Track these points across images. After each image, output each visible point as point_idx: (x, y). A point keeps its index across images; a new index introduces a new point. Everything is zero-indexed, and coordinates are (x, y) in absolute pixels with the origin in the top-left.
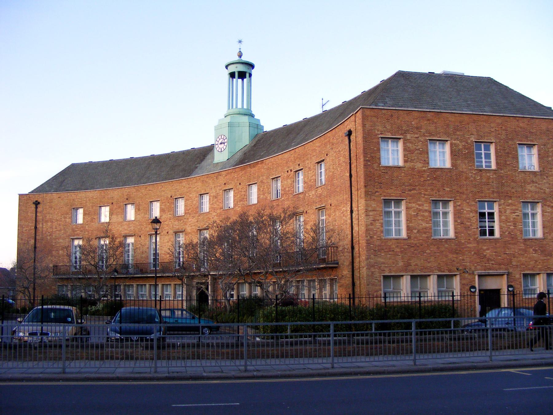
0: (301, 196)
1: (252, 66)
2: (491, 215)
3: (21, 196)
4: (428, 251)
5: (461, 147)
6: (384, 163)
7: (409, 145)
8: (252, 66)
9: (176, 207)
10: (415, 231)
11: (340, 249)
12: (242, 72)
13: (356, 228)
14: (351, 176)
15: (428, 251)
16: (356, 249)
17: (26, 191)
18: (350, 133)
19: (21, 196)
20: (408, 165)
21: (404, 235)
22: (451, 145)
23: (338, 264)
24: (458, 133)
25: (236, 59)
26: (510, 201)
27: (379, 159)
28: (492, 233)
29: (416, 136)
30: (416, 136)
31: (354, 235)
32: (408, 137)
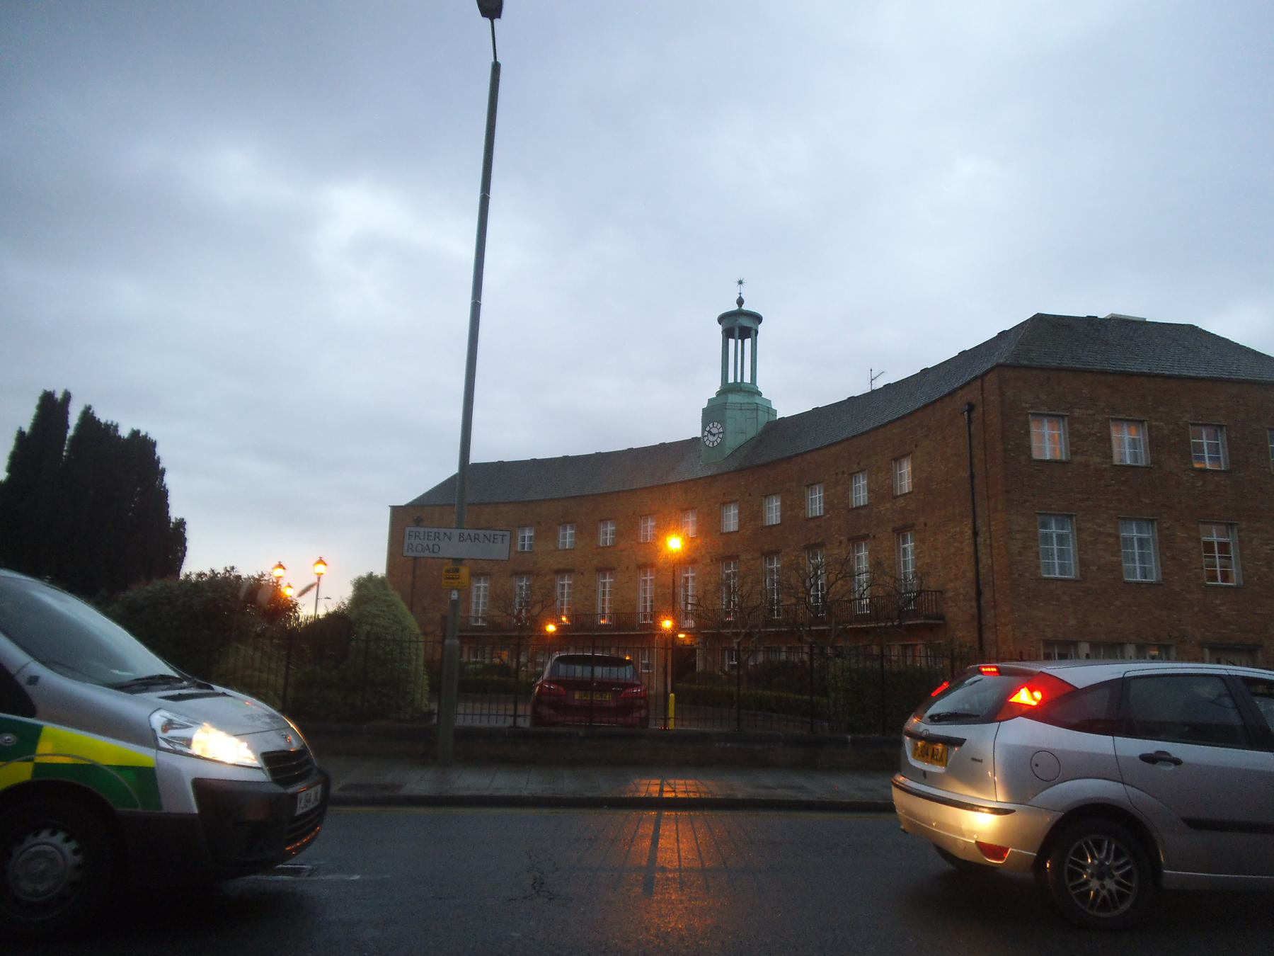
0: (863, 512)
1: (758, 319)
2: (1224, 548)
3: (396, 511)
4: (1118, 603)
5: (1166, 432)
6: (1036, 456)
7: (1078, 427)
8: (758, 319)
9: (848, 489)
10: (1095, 568)
11: (950, 594)
12: (739, 325)
13: (985, 560)
14: (972, 476)
15: (1118, 603)
16: (987, 594)
17: (403, 502)
18: (971, 408)
19: (396, 511)
20: (1078, 459)
21: (1073, 573)
22: (1150, 428)
23: (943, 618)
24: (1161, 409)
25: (736, 307)
26: (1258, 524)
27: (1029, 448)
28: (1226, 577)
29: (1090, 412)
30: (1090, 412)
31: (982, 571)
32: (1077, 413)
